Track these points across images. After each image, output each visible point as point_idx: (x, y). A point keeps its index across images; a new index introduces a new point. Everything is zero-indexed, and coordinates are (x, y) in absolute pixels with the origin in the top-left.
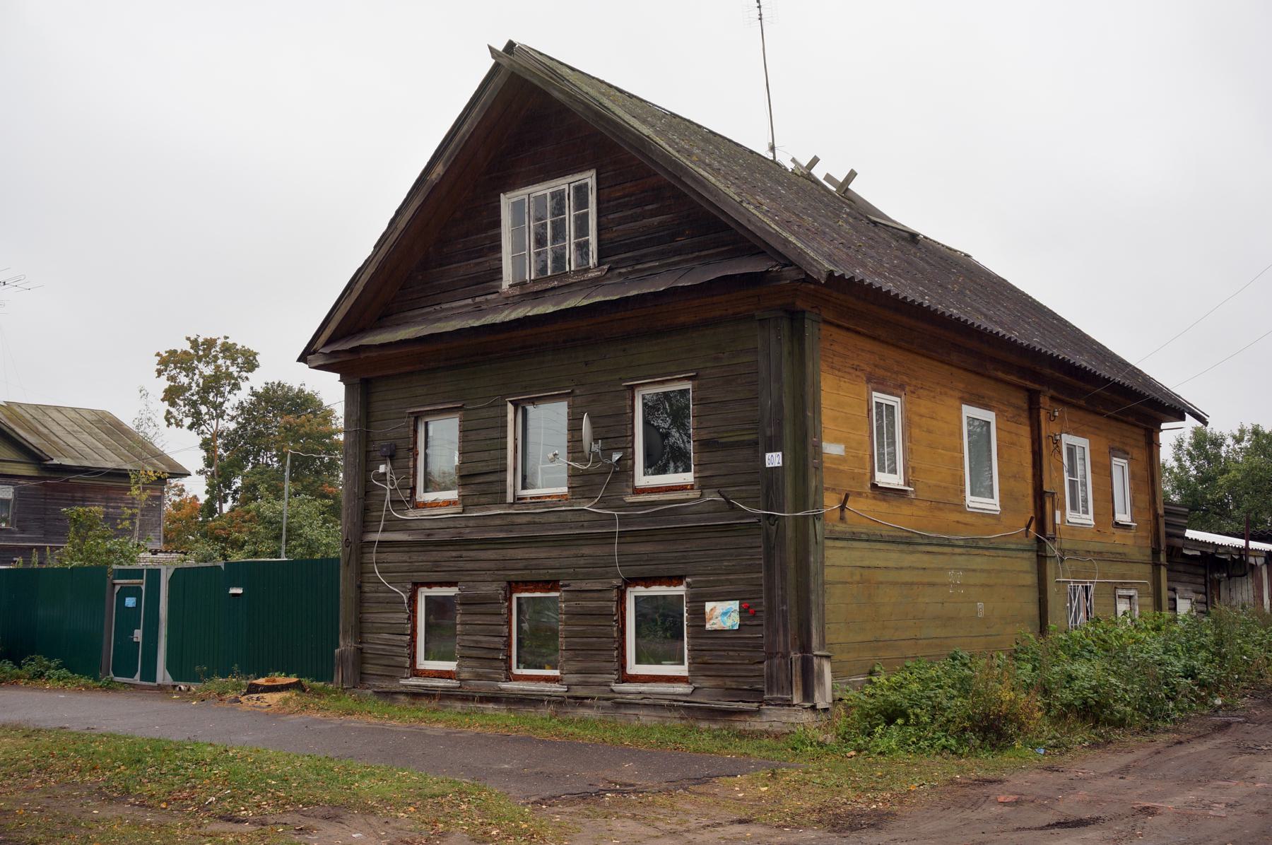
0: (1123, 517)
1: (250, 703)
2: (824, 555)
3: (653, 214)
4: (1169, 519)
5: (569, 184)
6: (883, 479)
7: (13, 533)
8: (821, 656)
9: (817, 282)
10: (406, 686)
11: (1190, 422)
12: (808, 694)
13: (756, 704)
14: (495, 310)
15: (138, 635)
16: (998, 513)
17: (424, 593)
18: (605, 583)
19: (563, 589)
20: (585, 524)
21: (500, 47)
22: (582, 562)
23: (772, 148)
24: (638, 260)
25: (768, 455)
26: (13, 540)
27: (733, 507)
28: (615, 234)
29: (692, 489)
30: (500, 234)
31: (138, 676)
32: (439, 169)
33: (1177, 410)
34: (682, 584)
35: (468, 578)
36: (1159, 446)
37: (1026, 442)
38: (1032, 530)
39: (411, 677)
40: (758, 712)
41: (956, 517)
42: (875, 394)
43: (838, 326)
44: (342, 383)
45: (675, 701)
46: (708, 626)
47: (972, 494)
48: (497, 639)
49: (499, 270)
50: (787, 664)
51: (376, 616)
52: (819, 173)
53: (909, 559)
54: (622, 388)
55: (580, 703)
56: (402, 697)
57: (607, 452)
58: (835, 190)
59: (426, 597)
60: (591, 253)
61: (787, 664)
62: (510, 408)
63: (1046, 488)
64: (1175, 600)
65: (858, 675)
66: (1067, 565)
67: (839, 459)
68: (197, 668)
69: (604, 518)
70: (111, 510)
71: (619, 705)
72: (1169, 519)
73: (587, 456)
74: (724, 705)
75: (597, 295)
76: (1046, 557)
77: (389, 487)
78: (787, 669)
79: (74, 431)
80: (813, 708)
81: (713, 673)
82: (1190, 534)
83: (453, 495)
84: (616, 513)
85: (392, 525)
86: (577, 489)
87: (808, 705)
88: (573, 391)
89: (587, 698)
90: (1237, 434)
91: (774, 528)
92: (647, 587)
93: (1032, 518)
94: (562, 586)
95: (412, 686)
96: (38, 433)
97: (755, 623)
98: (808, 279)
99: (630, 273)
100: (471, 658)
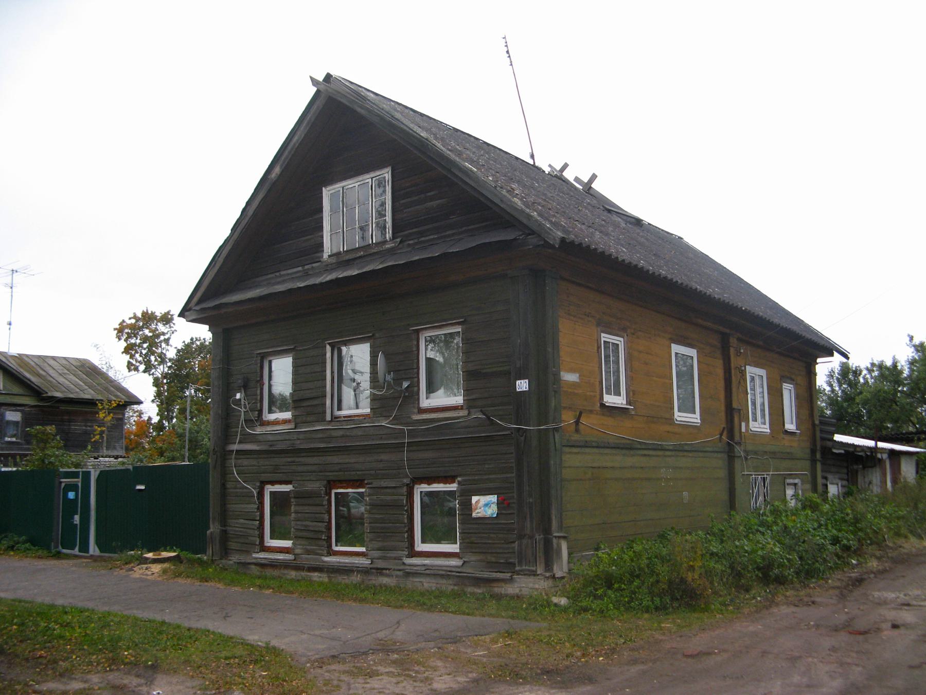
0: (790, 426)
1: (141, 572)
2: (561, 460)
3: (432, 199)
4: (822, 427)
5: (372, 178)
6: (610, 400)
7: (21, 444)
8: (559, 537)
9: (553, 247)
10: (256, 558)
11: (837, 359)
12: (548, 566)
13: (509, 574)
14: (319, 274)
15: (77, 519)
16: (699, 425)
17: (269, 489)
18: (398, 481)
19: (368, 486)
20: (384, 436)
21: (320, 78)
22: (381, 465)
23: (532, 156)
24: (421, 234)
25: (518, 382)
26: (22, 449)
27: (492, 423)
28: (405, 215)
29: (462, 409)
30: (322, 218)
31: (77, 549)
32: (277, 170)
33: (828, 349)
34: (454, 482)
35: (299, 478)
36: (816, 375)
37: (720, 372)
38: (724, 437)
39: (260, 551)
40: (511, 580)
41: (668, 428)
42: (603, 335)
43: (573, 282)
44: (210, 332)
45: (450, 571)
46: (474, 515)
47: (679, 411)
48: (320, 524)
49: (321, 245)
50: (533, 543)
51: (235, 507)
52: (569, 175)
53: (630, 461)
54: (409, 332)
55: (380, 573)
56: (253, 567)
57: (398, 381)
58: (581, 188)
59: (270, 492)
60: (387, 230)
61: (533, 543)
62: (328, 348)
63: (735, 405)
64: (826, 486)
65: (587, 550)
66: (750, 462)
67: (574, 385)
68: (114, 544)
69: (396, 431)
70: (89, 428)
71: (408, 574)
72: (822, 427)
73: (383, 385)
74: (486, 575)
75: (390, 261)
76: (734, 457)
77: (243, 410)
78: (533, 547)
79: (64, 373)
80: (553, 577)
81: (477, 551)
82: (838, 438)
83: (287, 415)
84: (405, 428)
85: (246, 438)
86: (377, 410)
87: (548, 574)
88: (373, 335)
89: (386, 569)
90: (869, 366)
91: (523, 438)
92: (429, 484)
93: (724, 428)
94: (367, 484)
95: (261, 558)
96: (39, 375)
97: (509, 512)
98: (547, 245)
99: (416, 244)
100: (302, 538)
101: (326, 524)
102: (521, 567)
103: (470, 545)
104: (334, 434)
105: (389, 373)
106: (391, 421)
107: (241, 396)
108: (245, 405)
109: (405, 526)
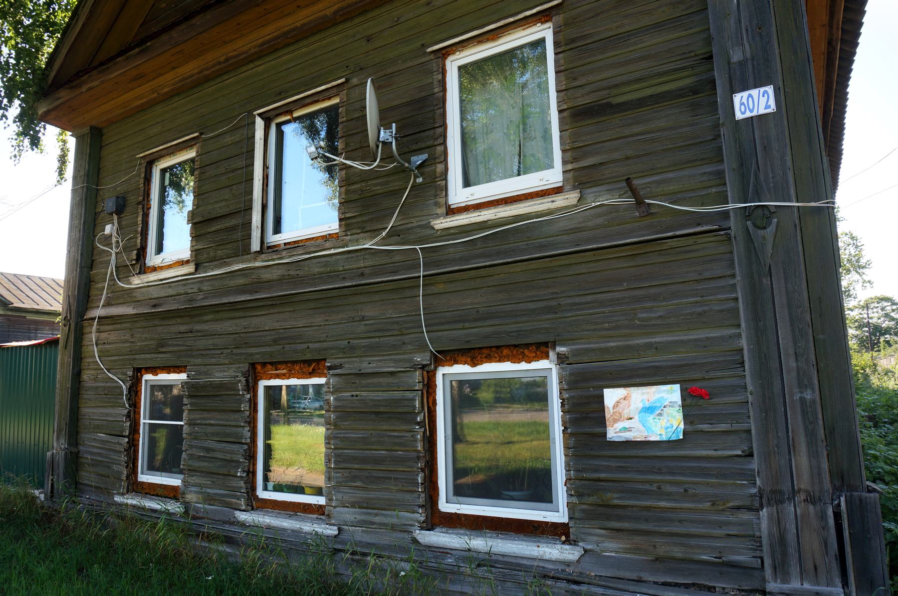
19: (331, 372)
35: (199, 361)
62: (259, 123)
94: (330, 368)
101: (246, 447)
102: (784, 581)
103: (778, 570)
104: (266, 276)
105: (388, 127)
106: (383, 238)
107: (112, 229)
108: (118, 242)
109: (419, 458)
